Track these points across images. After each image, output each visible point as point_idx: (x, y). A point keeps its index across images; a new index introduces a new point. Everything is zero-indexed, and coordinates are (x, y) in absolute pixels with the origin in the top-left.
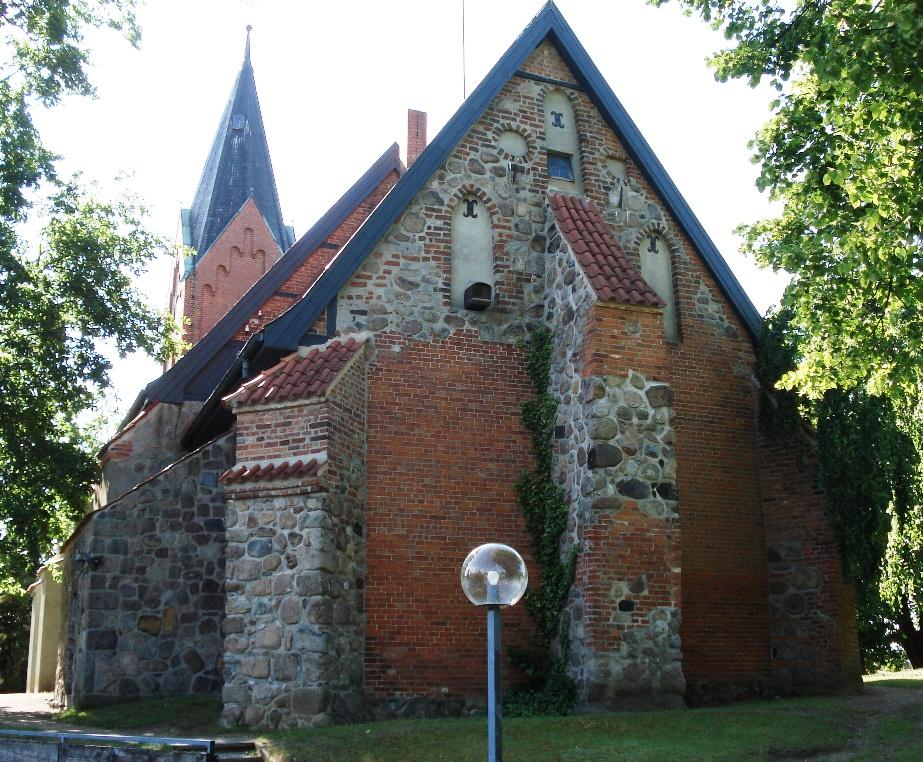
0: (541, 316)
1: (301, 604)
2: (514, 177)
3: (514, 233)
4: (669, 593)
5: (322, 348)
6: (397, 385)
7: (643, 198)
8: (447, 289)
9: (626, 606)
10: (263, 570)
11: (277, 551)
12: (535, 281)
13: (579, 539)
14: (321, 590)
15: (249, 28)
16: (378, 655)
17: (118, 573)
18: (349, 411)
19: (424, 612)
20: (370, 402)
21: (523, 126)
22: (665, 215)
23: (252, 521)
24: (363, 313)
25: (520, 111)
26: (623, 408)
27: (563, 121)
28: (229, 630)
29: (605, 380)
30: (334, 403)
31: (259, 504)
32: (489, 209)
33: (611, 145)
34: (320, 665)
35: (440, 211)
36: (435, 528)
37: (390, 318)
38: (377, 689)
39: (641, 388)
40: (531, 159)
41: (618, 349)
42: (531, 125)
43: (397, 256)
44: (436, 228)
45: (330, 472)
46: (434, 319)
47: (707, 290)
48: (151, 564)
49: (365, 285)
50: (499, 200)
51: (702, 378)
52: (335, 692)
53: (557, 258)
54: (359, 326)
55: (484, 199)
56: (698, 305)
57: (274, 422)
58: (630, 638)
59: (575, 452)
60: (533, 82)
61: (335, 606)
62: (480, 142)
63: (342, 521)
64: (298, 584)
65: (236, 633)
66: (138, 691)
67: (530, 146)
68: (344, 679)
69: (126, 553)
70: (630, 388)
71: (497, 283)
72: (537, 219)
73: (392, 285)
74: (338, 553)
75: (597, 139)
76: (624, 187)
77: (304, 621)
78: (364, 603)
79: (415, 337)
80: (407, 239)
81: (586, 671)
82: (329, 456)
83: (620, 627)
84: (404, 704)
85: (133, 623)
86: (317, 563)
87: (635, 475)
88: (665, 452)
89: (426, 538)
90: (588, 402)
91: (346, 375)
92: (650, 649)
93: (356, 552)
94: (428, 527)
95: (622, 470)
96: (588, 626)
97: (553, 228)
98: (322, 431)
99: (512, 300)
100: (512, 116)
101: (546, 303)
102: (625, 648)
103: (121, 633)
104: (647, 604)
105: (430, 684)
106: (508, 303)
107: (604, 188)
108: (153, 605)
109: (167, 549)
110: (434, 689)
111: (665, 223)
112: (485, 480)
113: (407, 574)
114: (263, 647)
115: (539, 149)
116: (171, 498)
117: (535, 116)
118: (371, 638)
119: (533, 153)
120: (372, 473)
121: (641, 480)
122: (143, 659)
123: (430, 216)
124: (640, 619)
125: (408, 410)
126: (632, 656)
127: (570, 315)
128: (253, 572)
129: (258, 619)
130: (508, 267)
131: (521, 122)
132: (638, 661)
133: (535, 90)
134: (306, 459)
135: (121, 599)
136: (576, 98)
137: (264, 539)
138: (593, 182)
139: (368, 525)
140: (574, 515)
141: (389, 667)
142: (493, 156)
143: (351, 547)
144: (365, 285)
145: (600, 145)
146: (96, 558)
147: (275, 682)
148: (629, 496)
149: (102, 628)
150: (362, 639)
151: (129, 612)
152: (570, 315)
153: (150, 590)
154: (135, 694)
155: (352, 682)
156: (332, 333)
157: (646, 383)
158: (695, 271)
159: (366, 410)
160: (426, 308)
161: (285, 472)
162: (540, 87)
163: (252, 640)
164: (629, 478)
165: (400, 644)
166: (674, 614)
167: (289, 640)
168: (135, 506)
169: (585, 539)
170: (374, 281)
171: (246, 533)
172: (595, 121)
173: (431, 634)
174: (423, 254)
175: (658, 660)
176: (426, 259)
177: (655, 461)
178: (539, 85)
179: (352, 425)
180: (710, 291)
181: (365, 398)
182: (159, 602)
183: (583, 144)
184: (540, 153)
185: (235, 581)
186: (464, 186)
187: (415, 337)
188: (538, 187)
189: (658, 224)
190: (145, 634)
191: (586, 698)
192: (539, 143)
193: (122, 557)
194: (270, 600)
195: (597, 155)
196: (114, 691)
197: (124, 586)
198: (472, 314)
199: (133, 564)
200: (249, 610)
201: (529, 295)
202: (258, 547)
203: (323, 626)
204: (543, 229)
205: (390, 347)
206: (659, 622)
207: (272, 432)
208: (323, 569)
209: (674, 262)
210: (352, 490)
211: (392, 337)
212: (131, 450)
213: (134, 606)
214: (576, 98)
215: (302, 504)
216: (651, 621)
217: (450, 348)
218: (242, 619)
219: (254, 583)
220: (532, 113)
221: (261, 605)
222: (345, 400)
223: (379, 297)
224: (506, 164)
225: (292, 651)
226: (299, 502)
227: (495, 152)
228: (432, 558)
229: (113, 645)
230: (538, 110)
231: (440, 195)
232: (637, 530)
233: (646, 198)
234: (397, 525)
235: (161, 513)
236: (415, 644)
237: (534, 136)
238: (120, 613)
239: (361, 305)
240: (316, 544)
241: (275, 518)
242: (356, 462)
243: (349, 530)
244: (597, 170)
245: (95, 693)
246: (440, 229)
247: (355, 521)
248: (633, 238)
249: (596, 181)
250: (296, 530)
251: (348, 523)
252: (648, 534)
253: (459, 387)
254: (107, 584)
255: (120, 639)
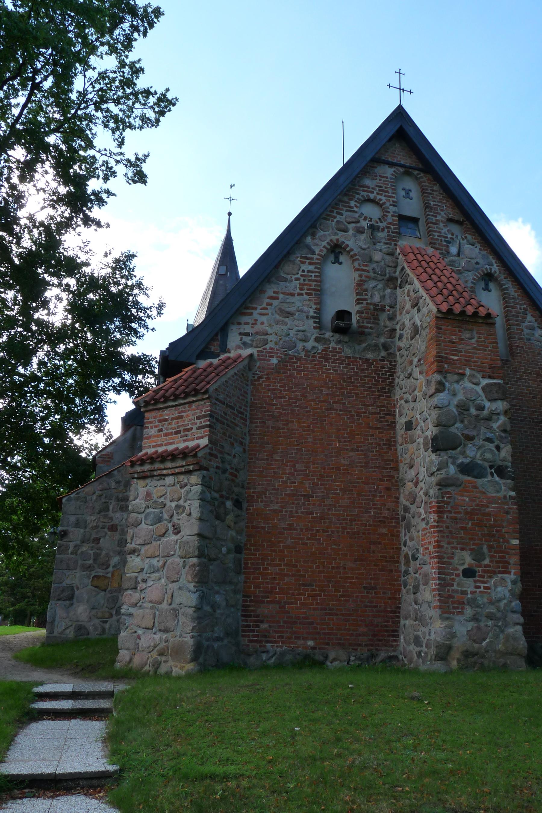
0: (394, 337)
1: (181, 565)
2: (372, 234)
3: (372, 275)
4: (508, 563)
5: (215, 361)
6: (274, 390)
7: (477, 250)
8: (319, 312)
9: (469, 573)
10: (155, 536)
11: (166, 520)
12: (389, 310)
13: (426, 513)
14: (197, 553)
15: (230, 214)
16: (252, 611)
17: (78, 542)
18: (232, 408)
19: (293, 575)
20: (252, 403)
21: (379, 197)
22: (496, 263)
23: (148, 495)
24: (247, 334)
25: (377, 186)
26: (462, 400)
27: (412, 194)
28: (125, 587)
29: (445, 377)
30: (217, 400)
31: (155, 482)
32: (352, 257)
33: (450, 210)
34: (193, 619)
35: (312, 259)
36: (304, 504)
37: (269, 338)
38: (251, 641)
39: (477, 384)
40: (385, 220)
41: (457, 352)
42: (385, 196)
43: (277, 293)
44: (308, 272)
45: (211, 454)
46: (305, 340)
47: (533, 319)
48: (105, 536)
49: (251, 314)
50: (359, 250)
51: (531, 387)
52: (207, 643)
53: (406, 290)
54: (245, 345)
55: (348, 249)
56: (526, 331)
57: (171, 416)
58: (472, 603)
59: (421, 441)
60: (387, 166)
61: (211, 567)
62: (345, 209)
63: (222, 496)
64: (180, 548)
65: (132, 589)
66: (88, 634)
67: (385, 211)
68: (218, 631)
69: (86, 527)
70: (467, 384)
71: (358, 312)
72: (391, 264)
73: (273, 314)
74: (217, 522)
75: (439, 206)
76: (462, 241)
77: (183, 581)
78: (243, 566)
79: (290, 352)
80: (285, 280)
81: (432, 631)
82: (210, 441)
83: (464, 593)
84: (274, 655)
85: (86, 581)
86: (195, 530)
87: (474, 458)
88: (501, 439)
89: (297, 512)
90: (430, 396)
91: (229, 379)
92: (492, 613)
93: (235, 523)
94: (298, 504)
95: (463, 453)
96: (434, 590)
97: (403, 268)
98: (205, 421)
99: (369, 325)
100: (370, 190)
101: (398, 328)
102: (469, 612)
103: (78, 589)
104: (488, 572)
105: (298, 638)
106: (367, 327)
107: (445, 241)
108: (105, 567)
109: (117, 526)
110: (301, 642)
111: (495, 268)
112: (347, 466)
113: (279, 542)
114: (150, 602)
115: (392, 213)
116: (122, 488)
117: (388, 190)
118: (248, 596)
119: (387, 216)
120: (252, 459)
121: (480, 462)
122: (93, 609)
123: (304, 263)
124: (482, 585)
125: (284, 410)
126: (475, 618)
127: (416, 330)
128: (146, 538)
129: (149, 577)
130: (366, 300)
131: (378, 194)
132: (482, 624)
133: (389, 171)
134: (191, 444)
135: (80, 562)
136: (422, 177)
137: (156, 510)
138: (436, 237)
139: (248, 501)
140: (421, 493)
141: (262, 622)
142: (355, 218)
143: (230, 518)
144: (251, 314)
145: (442, 210)
146: (63, 531)
147: (158, 633)
148: (469, 476)
149: (64, 584)
150: (239, 596)
151: (85, 573)
152: (416, 330)
153: (102, 556)
154: (85, 637)
155: (227, 634)
156: (224, 349)
157: (481, 380)
158: (522, 304)
159: (248, 409)
160: (299, 331)
161: (173, 456)
162: (393, 170)
163: (143, 595)
164: (468, 460)
165: (272, 602)
166: (514, 582)
167: (170, 596)
168: (94, 493)
169: (430, 513)
170: (259, 311)
171: (144, 506)
172: (437, 193)
173: (300, 594)
174: (298, 291)
175: (500, 624)
176: (300, 294)
177: (492, 446)
178: (391, 168)
179: (234, 419)
180: (536, 320)
181: (249, 400)
182: (109, 565)
183: (427, 210)
184: (392, 216)
185: (133, 545)
186: (331, 240)
187: (290, 352)
188: (391, 240)
189: (491, 269)
190: (96, 589)
191: (433, 657)
192: (392, 209)
193: (82, 531)
194: (158, 561)
195: (439, 218)
196: (70, 634)
197: (82, 553)
198: (337, 336)
199: (91, 535)
200: (142, 570)
201: (384, 321)
202: (152, 516)
203: (197, 585)
204: (395, 272)
205: (269, 360)
206: (499, 589)
207: (169, 424)
208: (199, 535)
209: (505, 297)
210: (233, 471)
211: (271, 353)
212: (112, 459)
213: (90, 568)
214: (422, 177)
215: (186, 481)
216: (493, 587)
217: (318, 361)
218: (136, 578)
219: (147, 547)
220: (386, 188)
221: (151, 566)
222: (228, 399)
223: (262, 323)
224: (365, 224)
225: (172, 607)
226: (183, 479)
227: (357, 215)
228: (302, 530)
229: (71, 598)
230: (392, 185)
231: (313, 247)
232: (477, 505)
233: (480, 249)
234: (271, 502)
235: (114, 498)
236: (285, 602)
237: (388, 204)
238: (79, 573)
239: (248, 329)
240: (196, 513)
241: (166, 493)
242: (238, 449)
243: (229, 504)
244: (440, 228)
245: (55, 634)
246: (312, 272)
247: (235, 497)
248: (470, 280)
249: (438, 236)
250: (181, 502)
251: (227, 498)
252: (488, 509)
253: (325, 391)
254: (70, 551)
255: (77, 593)
